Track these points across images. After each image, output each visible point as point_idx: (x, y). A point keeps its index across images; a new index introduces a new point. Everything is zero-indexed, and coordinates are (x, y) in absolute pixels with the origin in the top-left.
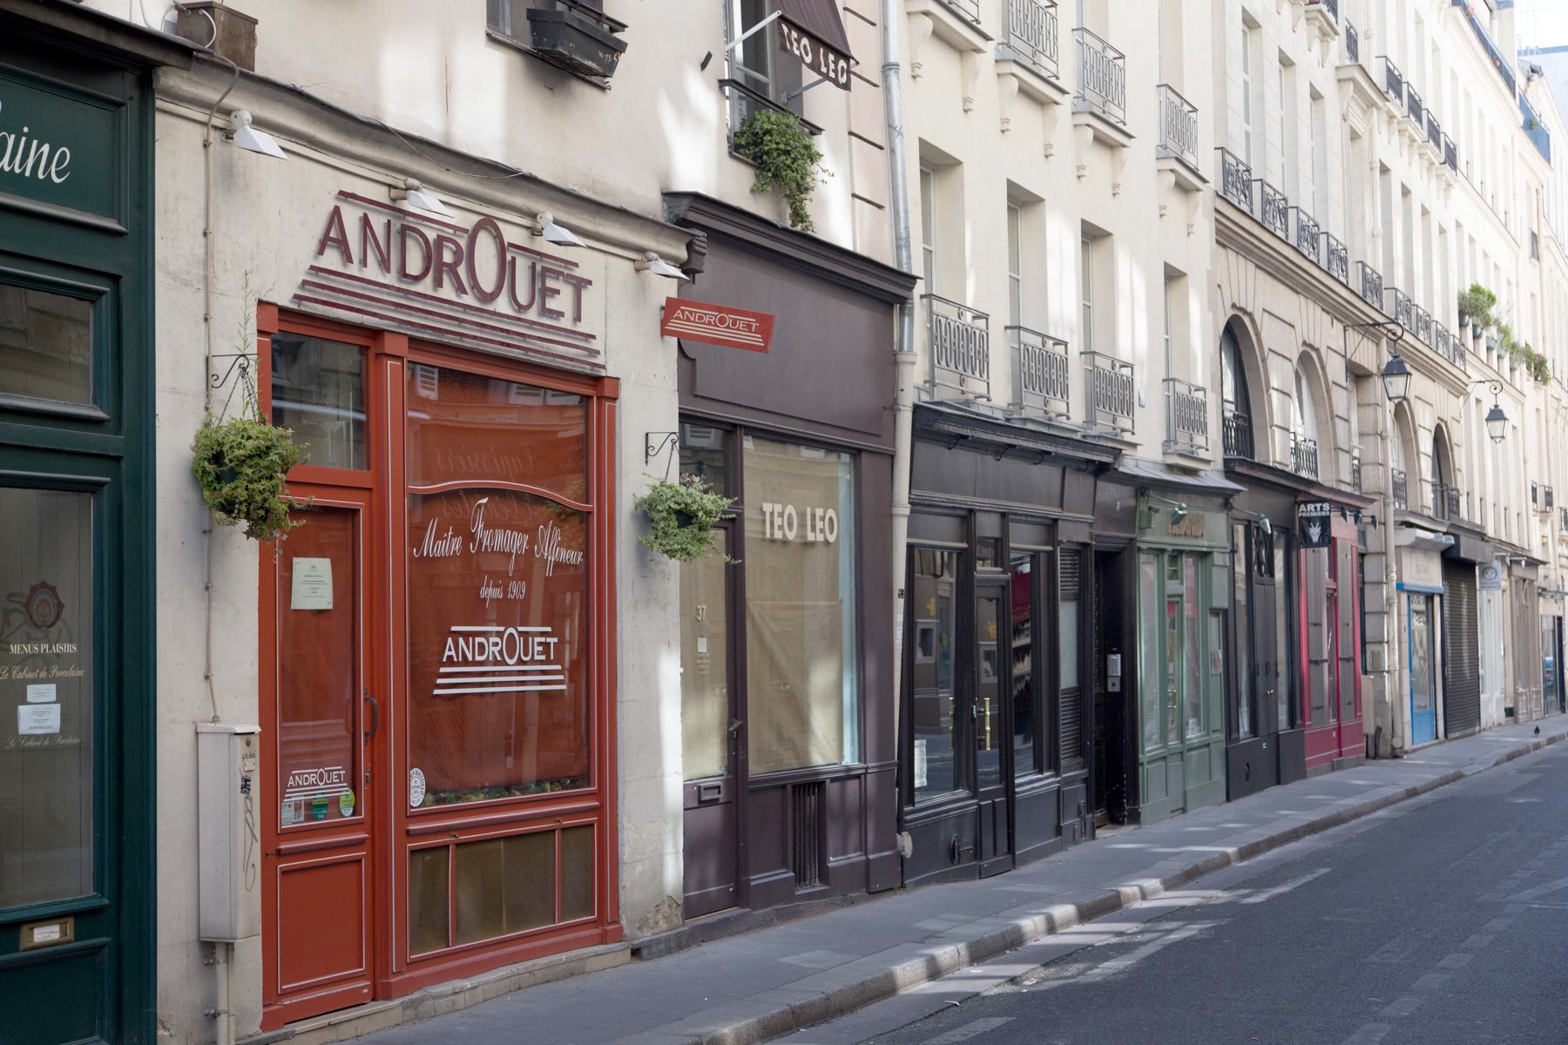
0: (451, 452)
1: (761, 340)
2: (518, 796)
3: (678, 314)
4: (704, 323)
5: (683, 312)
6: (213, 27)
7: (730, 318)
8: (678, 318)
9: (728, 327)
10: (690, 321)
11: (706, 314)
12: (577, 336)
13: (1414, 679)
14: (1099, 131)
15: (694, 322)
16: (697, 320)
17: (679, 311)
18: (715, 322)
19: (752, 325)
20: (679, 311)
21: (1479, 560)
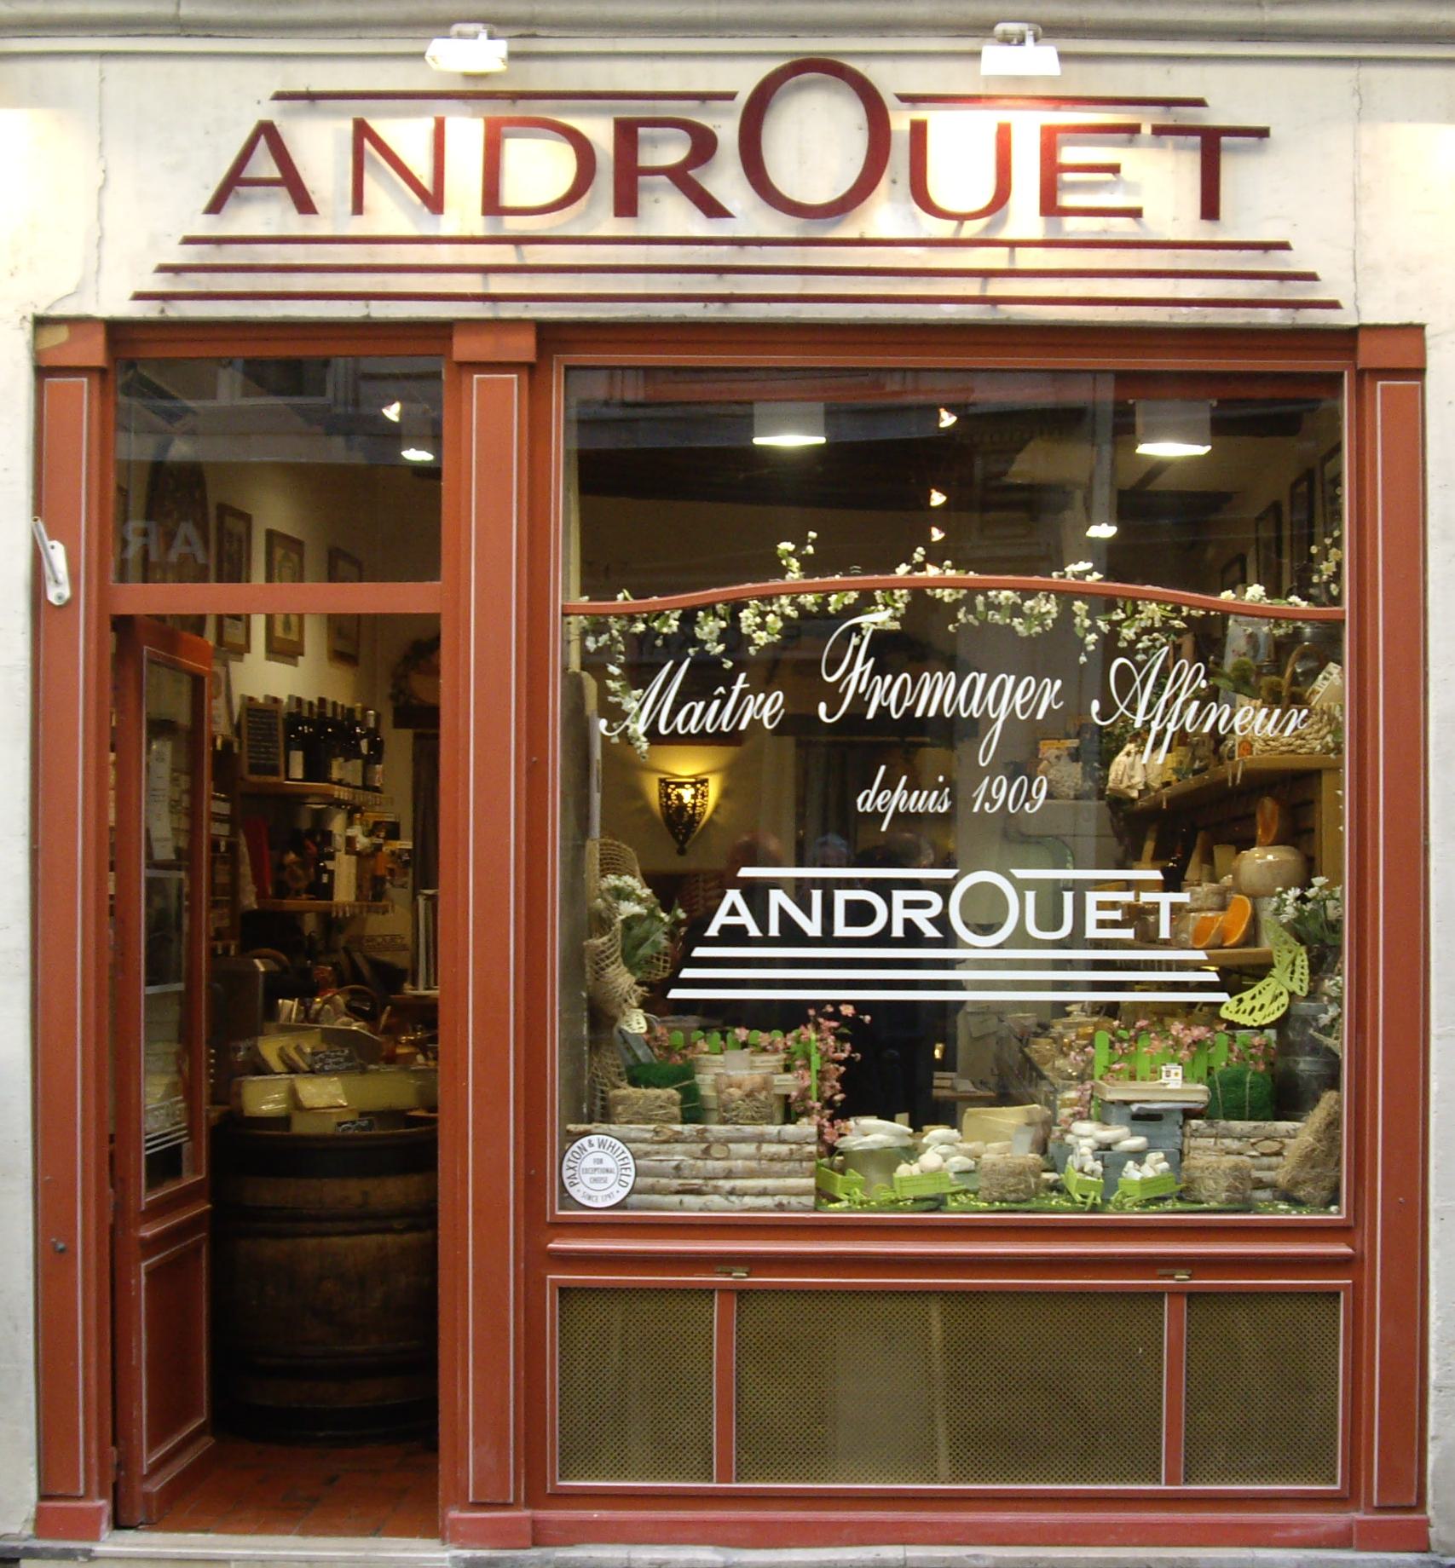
0: (742, 476)
1: (925, 793)
2: (557, 1422)
3: (732, 909)
4: (883, 939)
5: (756, 895)
6: (842, 661)
7: (1021, 886)
8: (734, 935)
9: (1020, 938)
10: (801, 939)
11: (884, 888)
12: (431, 915)
13: (659, 642)
14: (684, 604)
15: (828, 939)
16: (841, 930)
17: (733, 896)
18: (941, 921)
19: (1155, 909)
20: (733, 896)
21: (208, 612)
